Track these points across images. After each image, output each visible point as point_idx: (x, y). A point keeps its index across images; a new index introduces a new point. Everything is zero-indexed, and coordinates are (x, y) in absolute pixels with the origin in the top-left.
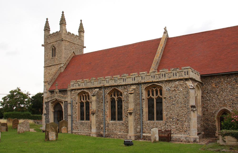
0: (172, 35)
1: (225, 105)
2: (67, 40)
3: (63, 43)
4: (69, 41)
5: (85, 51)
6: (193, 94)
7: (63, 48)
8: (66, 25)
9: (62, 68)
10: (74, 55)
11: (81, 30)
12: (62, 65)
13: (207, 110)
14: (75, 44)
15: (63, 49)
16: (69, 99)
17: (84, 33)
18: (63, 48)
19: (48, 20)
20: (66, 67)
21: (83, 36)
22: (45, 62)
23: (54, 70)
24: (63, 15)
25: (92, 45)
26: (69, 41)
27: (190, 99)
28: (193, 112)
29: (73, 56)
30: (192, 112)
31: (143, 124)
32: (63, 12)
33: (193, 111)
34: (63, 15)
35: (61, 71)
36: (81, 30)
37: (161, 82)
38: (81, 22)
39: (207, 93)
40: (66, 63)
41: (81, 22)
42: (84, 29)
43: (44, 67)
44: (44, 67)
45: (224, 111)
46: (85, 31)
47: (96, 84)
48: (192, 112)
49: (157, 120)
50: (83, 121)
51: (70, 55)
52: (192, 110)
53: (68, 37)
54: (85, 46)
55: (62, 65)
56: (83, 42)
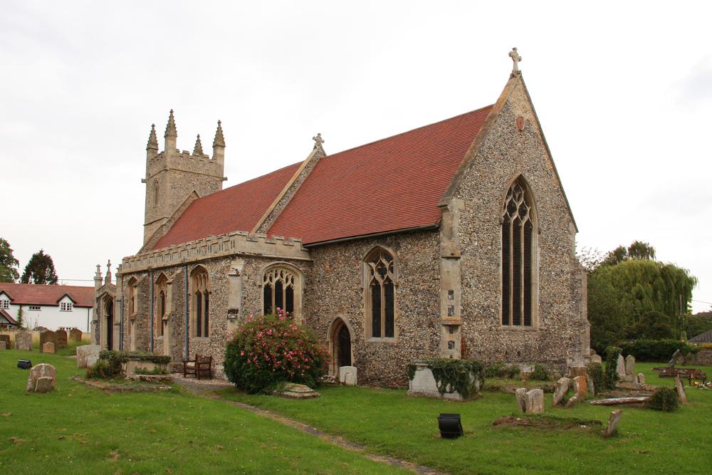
0: (330, 149)
1: (341, 310)
2: (180, 167)
3: (168, 176)
4: (182, 171)
5: (225, 185)
6: (236, 286)
7: (169, 185)
8: (177, 138)
9: (164, 228)
10: (196, 198)
11: (219, 143)
12: (164, 222)
13: (319, 319)
14: (198, 174)
15: (169, 188)
16: (118, 293)
17: (225, 148)
18: (169, 185)
19: (155, 128)
20: (173, 226)
21: (223, 156)
22: (146, 214)
23: (156, 227)
24: (171, 117)
25: (240, 169)
26: (184, 169)
27: (231, 297)
28: (231, 321)
29: (194, 201)
30: (229, 321)
31: (188, 342)
32: (172, 112)
33: (232, 320)
34: (171, 117)
35: (162, 234)
36: (219, 143)
37: (203, 261)
38: (219, 125)
39: (319, 282)
40: (175, 217)
41: (219, 125)
42: (225, 140)
43: (145, 225)
44: (145, 225)
45: (338, 325)
46: (226, 145)
47: (176, 260)
48: (229, 321)
49: (386, 336)
50: (378, 339)
51: (184, 196)
52: (228, 318)
53: (181, 161)
54: (225, 176)
55: (164, 222)
56: (221, 167)
